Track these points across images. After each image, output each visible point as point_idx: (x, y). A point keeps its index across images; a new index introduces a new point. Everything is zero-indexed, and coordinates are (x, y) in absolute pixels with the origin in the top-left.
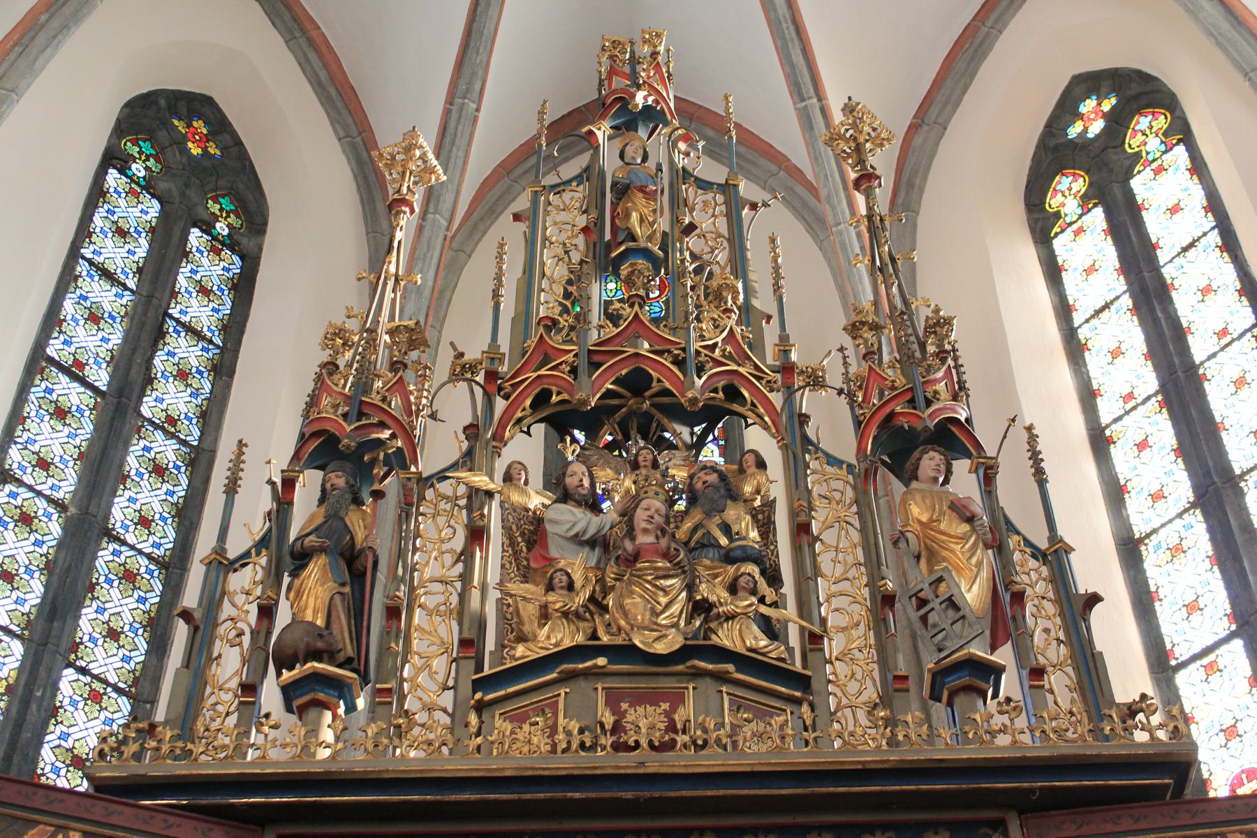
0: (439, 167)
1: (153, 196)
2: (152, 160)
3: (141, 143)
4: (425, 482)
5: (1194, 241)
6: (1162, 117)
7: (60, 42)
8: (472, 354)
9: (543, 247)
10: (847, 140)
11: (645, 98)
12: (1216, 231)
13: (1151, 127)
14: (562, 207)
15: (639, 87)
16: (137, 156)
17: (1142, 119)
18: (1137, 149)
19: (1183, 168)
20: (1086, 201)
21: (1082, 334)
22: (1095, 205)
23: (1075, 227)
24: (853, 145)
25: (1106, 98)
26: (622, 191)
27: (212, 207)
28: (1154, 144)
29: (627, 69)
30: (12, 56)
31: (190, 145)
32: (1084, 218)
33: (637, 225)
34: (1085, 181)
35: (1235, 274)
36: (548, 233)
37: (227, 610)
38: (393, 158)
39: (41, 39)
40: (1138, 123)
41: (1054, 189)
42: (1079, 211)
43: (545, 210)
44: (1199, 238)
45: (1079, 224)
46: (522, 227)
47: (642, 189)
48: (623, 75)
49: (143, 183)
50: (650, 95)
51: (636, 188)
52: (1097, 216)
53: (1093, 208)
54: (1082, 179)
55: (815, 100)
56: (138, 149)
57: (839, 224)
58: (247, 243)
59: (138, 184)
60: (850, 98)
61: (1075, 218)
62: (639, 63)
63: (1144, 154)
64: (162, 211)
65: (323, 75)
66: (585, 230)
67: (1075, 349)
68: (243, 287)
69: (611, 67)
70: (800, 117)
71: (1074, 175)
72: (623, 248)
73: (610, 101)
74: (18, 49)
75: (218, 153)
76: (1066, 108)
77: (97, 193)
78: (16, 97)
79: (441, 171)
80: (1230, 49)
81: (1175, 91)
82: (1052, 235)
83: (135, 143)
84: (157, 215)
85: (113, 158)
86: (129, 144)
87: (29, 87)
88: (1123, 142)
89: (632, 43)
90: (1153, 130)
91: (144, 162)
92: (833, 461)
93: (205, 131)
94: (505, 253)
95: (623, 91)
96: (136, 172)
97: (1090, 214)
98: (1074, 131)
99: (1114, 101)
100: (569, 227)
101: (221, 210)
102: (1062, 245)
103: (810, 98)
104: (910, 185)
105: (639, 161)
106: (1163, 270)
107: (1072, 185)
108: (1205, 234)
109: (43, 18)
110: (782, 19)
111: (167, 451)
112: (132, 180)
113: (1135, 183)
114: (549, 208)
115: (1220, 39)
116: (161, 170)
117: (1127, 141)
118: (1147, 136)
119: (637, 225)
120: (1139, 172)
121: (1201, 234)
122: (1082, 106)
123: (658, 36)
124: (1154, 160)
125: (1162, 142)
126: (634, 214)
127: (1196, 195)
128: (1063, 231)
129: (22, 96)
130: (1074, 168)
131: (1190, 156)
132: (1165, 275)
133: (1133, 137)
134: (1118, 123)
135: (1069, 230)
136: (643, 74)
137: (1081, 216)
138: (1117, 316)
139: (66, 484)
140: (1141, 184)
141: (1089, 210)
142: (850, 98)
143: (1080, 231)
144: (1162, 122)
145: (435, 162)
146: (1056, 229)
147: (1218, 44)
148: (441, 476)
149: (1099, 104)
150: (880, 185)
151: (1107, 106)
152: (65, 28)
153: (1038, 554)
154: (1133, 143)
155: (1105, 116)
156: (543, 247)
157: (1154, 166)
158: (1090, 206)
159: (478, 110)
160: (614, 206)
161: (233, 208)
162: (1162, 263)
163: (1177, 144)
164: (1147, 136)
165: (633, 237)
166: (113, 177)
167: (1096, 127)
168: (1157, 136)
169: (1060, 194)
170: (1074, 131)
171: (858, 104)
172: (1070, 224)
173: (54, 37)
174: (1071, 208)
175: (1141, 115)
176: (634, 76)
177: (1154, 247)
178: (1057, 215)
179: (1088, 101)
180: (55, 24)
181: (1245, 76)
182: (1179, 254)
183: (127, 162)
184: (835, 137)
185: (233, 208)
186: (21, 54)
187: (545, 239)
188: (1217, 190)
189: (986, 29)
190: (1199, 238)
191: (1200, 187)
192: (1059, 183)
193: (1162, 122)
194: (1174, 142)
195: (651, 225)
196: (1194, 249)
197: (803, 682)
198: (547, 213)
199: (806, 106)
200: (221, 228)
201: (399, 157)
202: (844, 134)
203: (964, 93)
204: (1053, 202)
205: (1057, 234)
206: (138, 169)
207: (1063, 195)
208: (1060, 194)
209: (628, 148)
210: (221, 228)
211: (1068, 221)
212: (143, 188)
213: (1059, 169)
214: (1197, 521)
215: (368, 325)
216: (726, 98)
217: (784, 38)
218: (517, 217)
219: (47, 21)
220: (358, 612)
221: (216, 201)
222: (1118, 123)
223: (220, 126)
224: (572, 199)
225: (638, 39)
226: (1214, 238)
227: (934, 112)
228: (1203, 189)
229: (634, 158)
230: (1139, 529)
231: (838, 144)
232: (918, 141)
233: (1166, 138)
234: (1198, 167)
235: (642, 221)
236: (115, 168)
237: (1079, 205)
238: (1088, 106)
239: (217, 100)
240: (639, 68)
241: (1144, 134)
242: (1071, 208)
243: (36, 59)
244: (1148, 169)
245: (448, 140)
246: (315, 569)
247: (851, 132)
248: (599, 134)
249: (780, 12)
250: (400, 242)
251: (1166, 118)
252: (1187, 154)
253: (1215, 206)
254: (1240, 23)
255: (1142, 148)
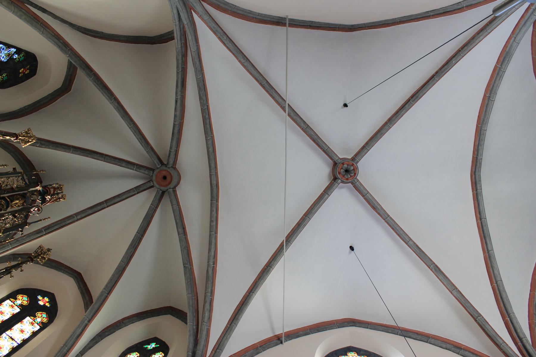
0: (26, 145)
1: (8, 60)
2: (18, 60)
3: (23, 57)
5: (14, 340)
6: (46, 320)
7: (56, 45)
9: (7, 177)
10: (41, 252)
11: (48, 198)
12: (17, 345)
13: (43, 318)
14: (18, 180)
15: (51, 196)
16: (20, 56)
17: (45, 315)
18: (37, 316)
19: (33, 330)
20: (21, 306)
22: (20, 309)
23: (13, 305)
24: (40, 253)
25: (49, 304)
26: (23, 196)
27: (5, 75)
28: (39, 320)
29: (56, 192)
30: (51, 33)
31: (23, 69)
32: (16, 306)
33: (15, 202)
34: (26, 304)
35: (5, 354)
36: (11, 178)
38: (29, 134)
39: (56, 41)
40: (44, 314)
41: (23, 296)
42: (18, 305)
43: (17, 176)
44: (15, 341)
45: (15, 306)
46: (11, 170)
47: (25, 202)
48: (54, 191)
49: (12, 57)
50: (49, 199)
51: (25, 200)
52: (17, 310)
53: (20, 308)
54: (27, 303)
55: (45, 233)
56: (21, 56)
57: (11, 245)
59: (12, 56)
60: (51, 249)
61: (16, 304)
62: (57, 195)
63: (36, 318)
64: (3, 62)
66: (12, 188)
69: (56, 188)
70: (39, 229)
71: (28, 300)
72: (8, 200)
73: (47, 188)
74: (53, 34)
75: (20, 76)
76: (45, 294)
77: (9, 46)
78: (41, 33)
79: (25, 146)
80: (71, 339)
81: (54, 322)
82: (10, 299)
83: (23, 56)
84: (2, 61)
85: (19, 51)
86: (23, 54)
87: (44, 37)
88: (38, 312)
89: (62, 192)
90: (43, 319)
91: (18, 58)
93: (26, 73)
94: (4, 167)
95: (50, 192)
96: (15, 56)
97: (17, 308)
98: (40, 297)
99: (49, 306)
100: (13, 183)
101: (4, 77)
102: (8, 302)
103: (45, 232)
105: (32, 199)
106: (4, 333)
107: (25, 301)
108: (16, 342)
109: (61, 41)
110: (65, 222)
112: (12, 55)
113: (28, 318)
114: (17, 177)
115: (73, 336)
116: (16, 62)
117: (39, 312)
118: (41, 317)
119: (15, 202)
120: (31, 318)
121: (16, 341)
122: (46, 298)
123: (64, 199)
124: (35, 321)
125: (40, 322)
126: (18, 201)
127: (26, 336)
128: (12, 302)
129: (41, 35)
130: (29, 300)
131: (37, 331)
132: (3, 335)
133: (21, 296)
134: (43, 309)
135: (12, 303)
136: (55, 197)
137: (17, 305)
138: (11, 344)
140: (28, 319)
141: (19, 308)
142: (51, 249)
143: (12, 306)
144: (45, 320)
145: (28, 144)
146: (12, 300)
147: (72, 335)
149: (47, 302)
150: (30, 263)
151: (48, 305)
152: (59, 47)
154: (39, 314)
155: (44, 305)
156: (7, 177)
157: (33, 322)
158: (20, 307)
159: (36, 146)
160: (19, 194)
161: (4, 80)
162: (6, 332)
163: (40, 326)
164: (41, 317)
165: (12, 201)
166: (14, 50)
167: (41, 303)
168: (41, 320)
169: (22, 298)
170: (40, 297)
171: (50, 252)
172: (14, 303)
173: (57, 44)
174: (19, 302)
175: (46, 314)
176: (54, 194)
178: (16, 299)
179: (48, 299)
180: (60, 44)
181: (64, 344)
182: (9, 336)
183: (18, 54)
184: (42, 248)
185: (4, 80)
186: (52, 35)
187: (9, 177)
188: (29, 341)
189: (63, 269)
190: (15, 341)
191: (29, 336)
192: (25, 297)
193: (45, 320)
194: (40, 325)
195: (15, 206)
196: (12, 340)
198: (16, 177)
199: (43, 231)
201: (29, 135)
202: (42, 251)
203: (47, 267)
204: (20, 297)
205: (10, 300)
206: (16, 56)
207: (22, 299)
208: (22, 298)
209: (35, 196)
211: (15, 302)
212: (10, 57)
213: (29, 296)
215: (37, 200)
216: (49, 218)
217: (61, 224)
218: (14, 169)
219: (61, 42)
221: (6, 76)
222: (43, 309)
223: (27, 77)
224: (20, 183)
225: (63, 194)
226: (15, 345)
228: (29, 337)
229: (32, 198)
231: (40, 250)
233: (41, 323)
234: (34, 334)
235: (17, 203)
236: (16, 51)
237: (20, 304)
238: (46, 299)
239: (35, 76)
240: (56, 195)
241: (41, 316)
242: (19, 302)
243: (51, 39)
244: (32, 320)
247: (43, 252)
248: (38, 187)
249: (68, 222)
250: (6, 138)
251: (46, 321)
252: (37, 330)
253: (25, 342)
254: (77, 338)
255: (38, 317)
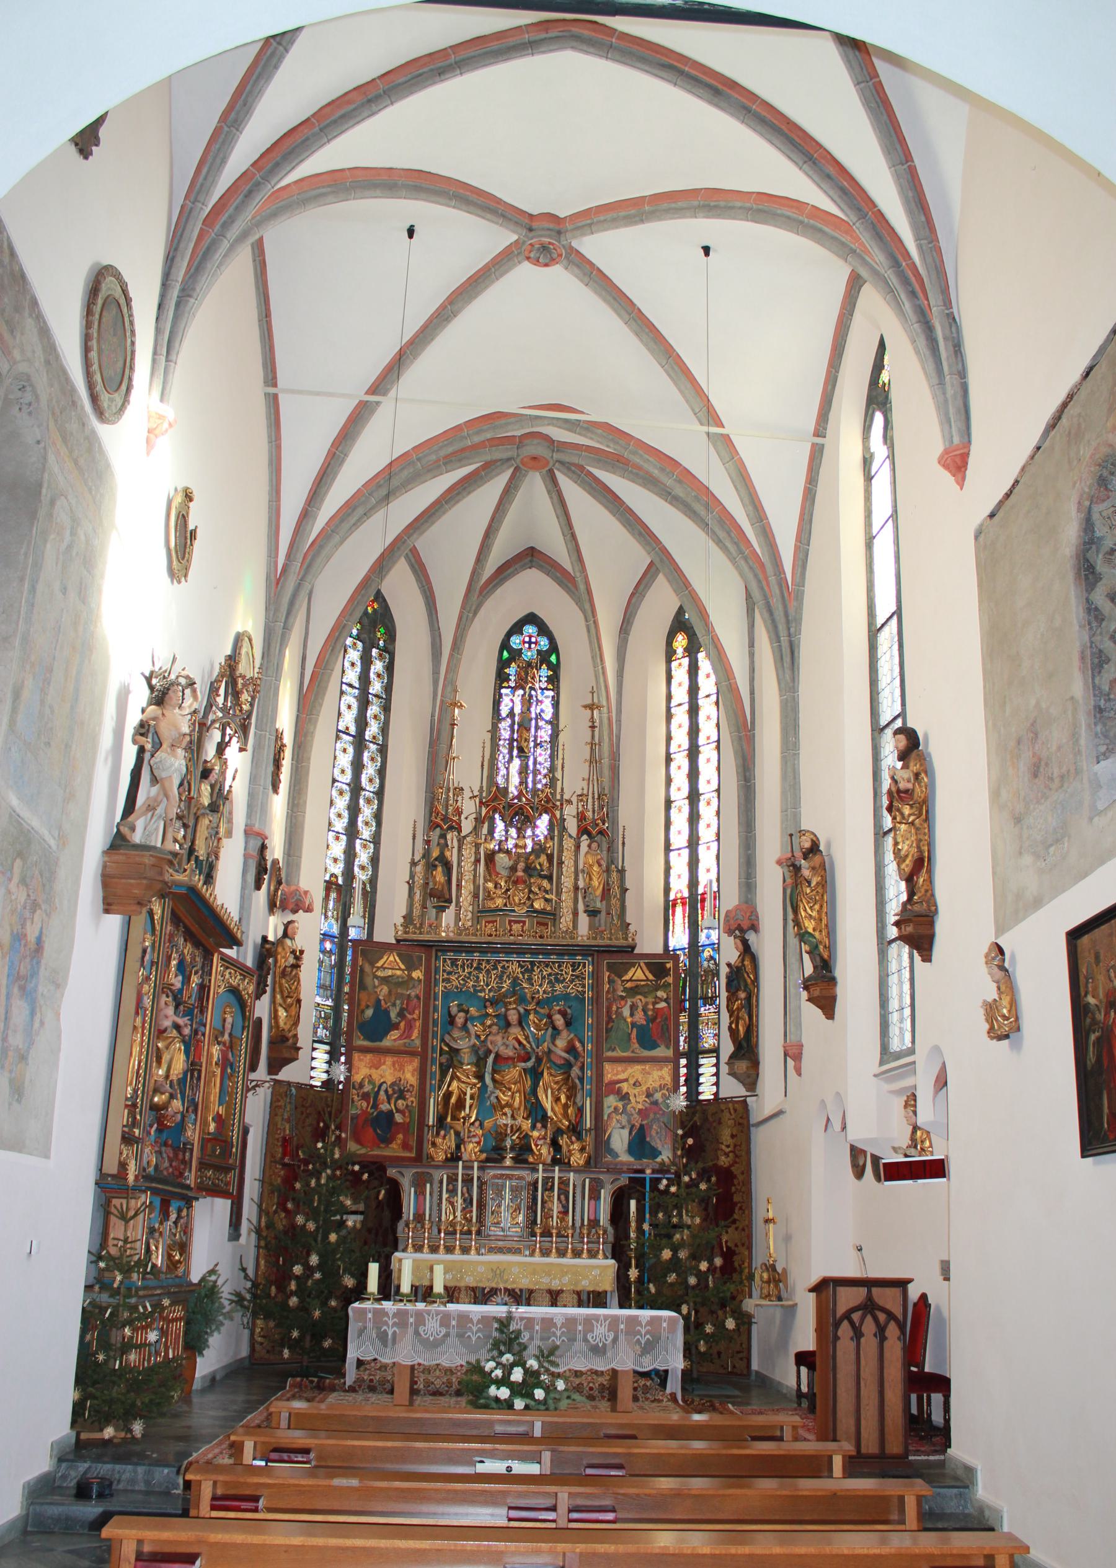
4: (464, 837)
8: (476, 793)
21: (673, 711)
37: (416, 878)
58: (390, 647)
65: (413, 560)
67: (669, 716)
68: (390, 668)
92: (570, 836)
102: (674, 664)
104: (628, 622)
111: (373, 747)
139: (348, 777)
148: (467, 836)
153: (618, 871)
177: (698, 689)
197: (554, 915)
200: (381, 643)
204: (675, 645)
210: (381, 643)
214: (687, 802)
220: (449, 881)
227: (642, 587)
230: (672, 799)
232: (634, 600)
245: (462, 626)
246: (440, 869)
